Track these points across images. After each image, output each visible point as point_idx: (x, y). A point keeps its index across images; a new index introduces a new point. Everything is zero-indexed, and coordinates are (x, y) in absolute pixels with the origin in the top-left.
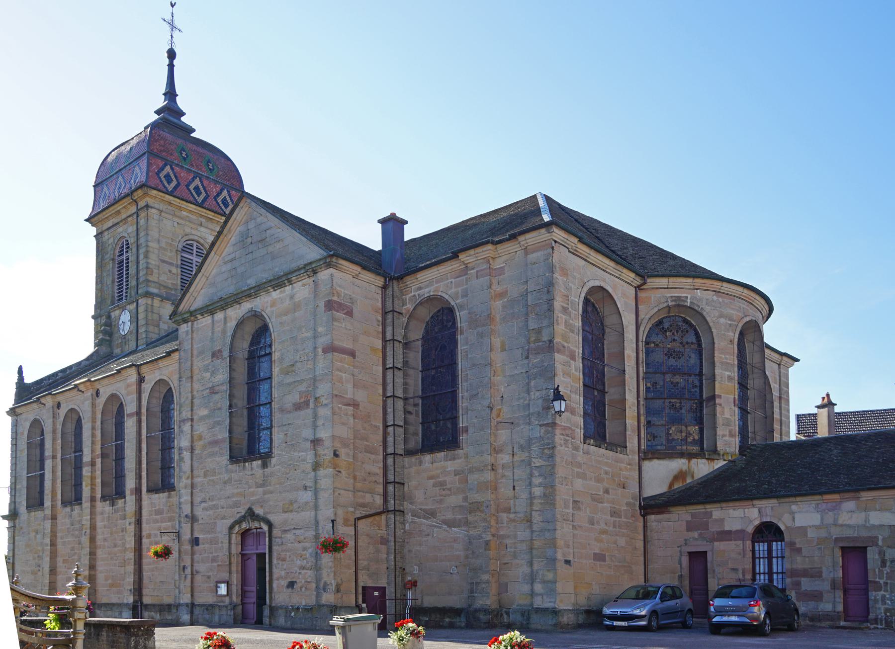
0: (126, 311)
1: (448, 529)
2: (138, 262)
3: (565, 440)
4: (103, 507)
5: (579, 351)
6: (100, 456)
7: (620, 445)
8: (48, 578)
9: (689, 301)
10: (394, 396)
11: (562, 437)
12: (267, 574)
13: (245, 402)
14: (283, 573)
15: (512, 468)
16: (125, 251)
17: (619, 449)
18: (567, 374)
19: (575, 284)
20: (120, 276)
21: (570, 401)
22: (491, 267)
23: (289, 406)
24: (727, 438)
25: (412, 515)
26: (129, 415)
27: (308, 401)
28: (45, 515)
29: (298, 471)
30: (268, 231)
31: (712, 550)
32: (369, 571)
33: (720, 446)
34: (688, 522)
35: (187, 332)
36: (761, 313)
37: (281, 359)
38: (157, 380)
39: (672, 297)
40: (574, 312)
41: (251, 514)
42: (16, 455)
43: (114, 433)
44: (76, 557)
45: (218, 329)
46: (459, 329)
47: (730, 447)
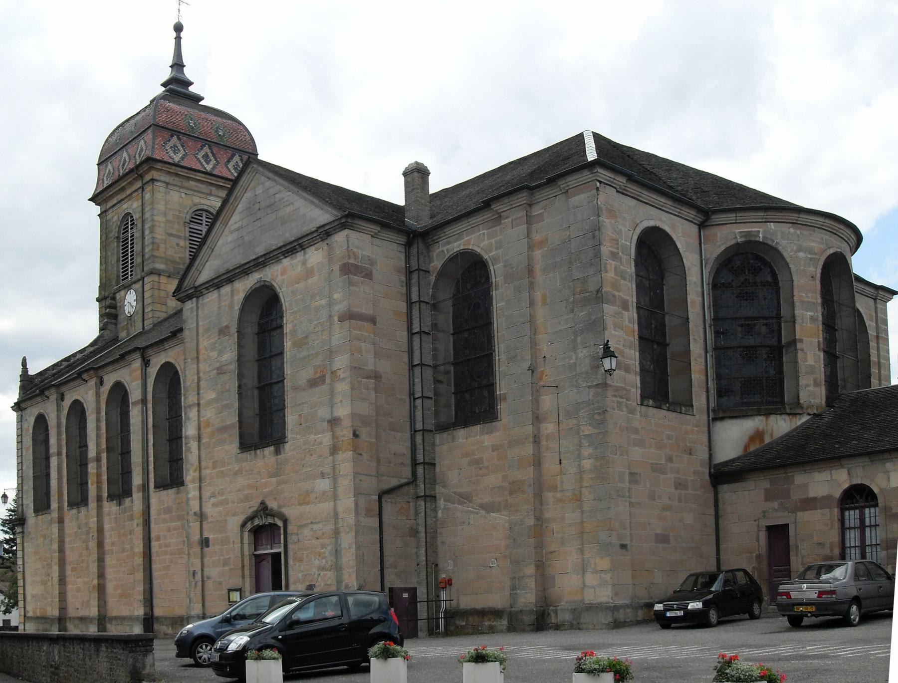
0: (132, 290)
1: (486, 515)
2: (143, 238)
3: (619, 402)
4: (110, 508)
5: (632, 299)
6: (105, 451)
7: (683, 405)
8: (58, 589)
9: (761, 236)
10: (421, 365)
11: (614, 399)
12: (283, 577)
13: (256, 380)
14: (300, 575)
15: (557, 438)
16: (130, 227)
17: (683, 409)
18: (616, 326)
19: (625, 227)
20: (125, 254)
21: (623, 356)
22: (528, 214)
23: (303, 382)
24: (811, 388)
25: (445, 501)
26: (134, 404)
27: (324, 376)
28: (52, 518)
29: (314, 456)
30: (277, 196)
31: (795, 523)
32: (396, 569)
33: (804, 398)
34: (766, 490)
35: (192, 308)
36: (848, 243)
37: (294, 332)
38: (162, 363)
39: (740, 232)
40: (625, 257)
41: (264, 509)
42: (22, 453)
43: (119, 424)
44: (84, 565)
45: (226, 302)
46: (494, 284)
47: (814, 399)
